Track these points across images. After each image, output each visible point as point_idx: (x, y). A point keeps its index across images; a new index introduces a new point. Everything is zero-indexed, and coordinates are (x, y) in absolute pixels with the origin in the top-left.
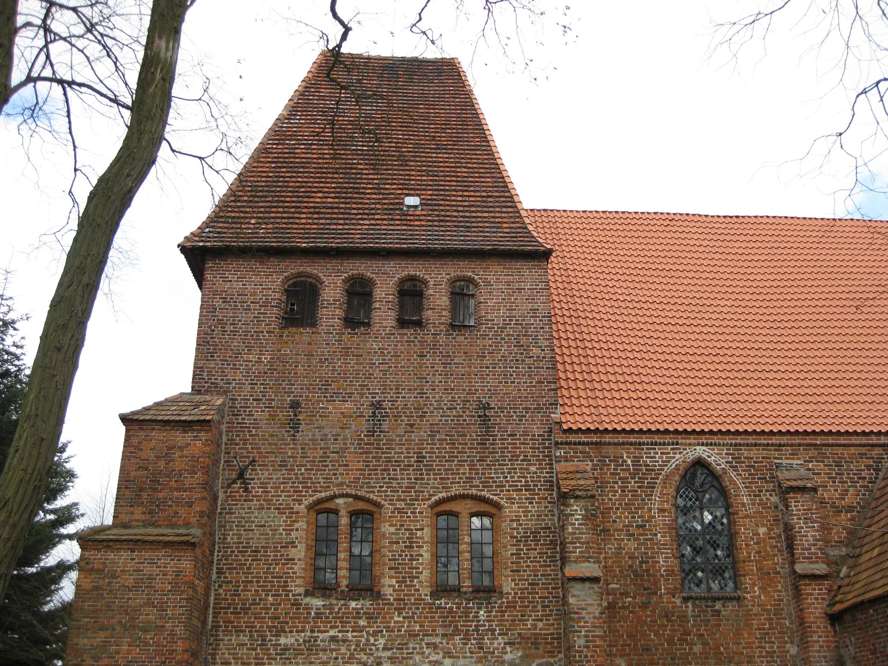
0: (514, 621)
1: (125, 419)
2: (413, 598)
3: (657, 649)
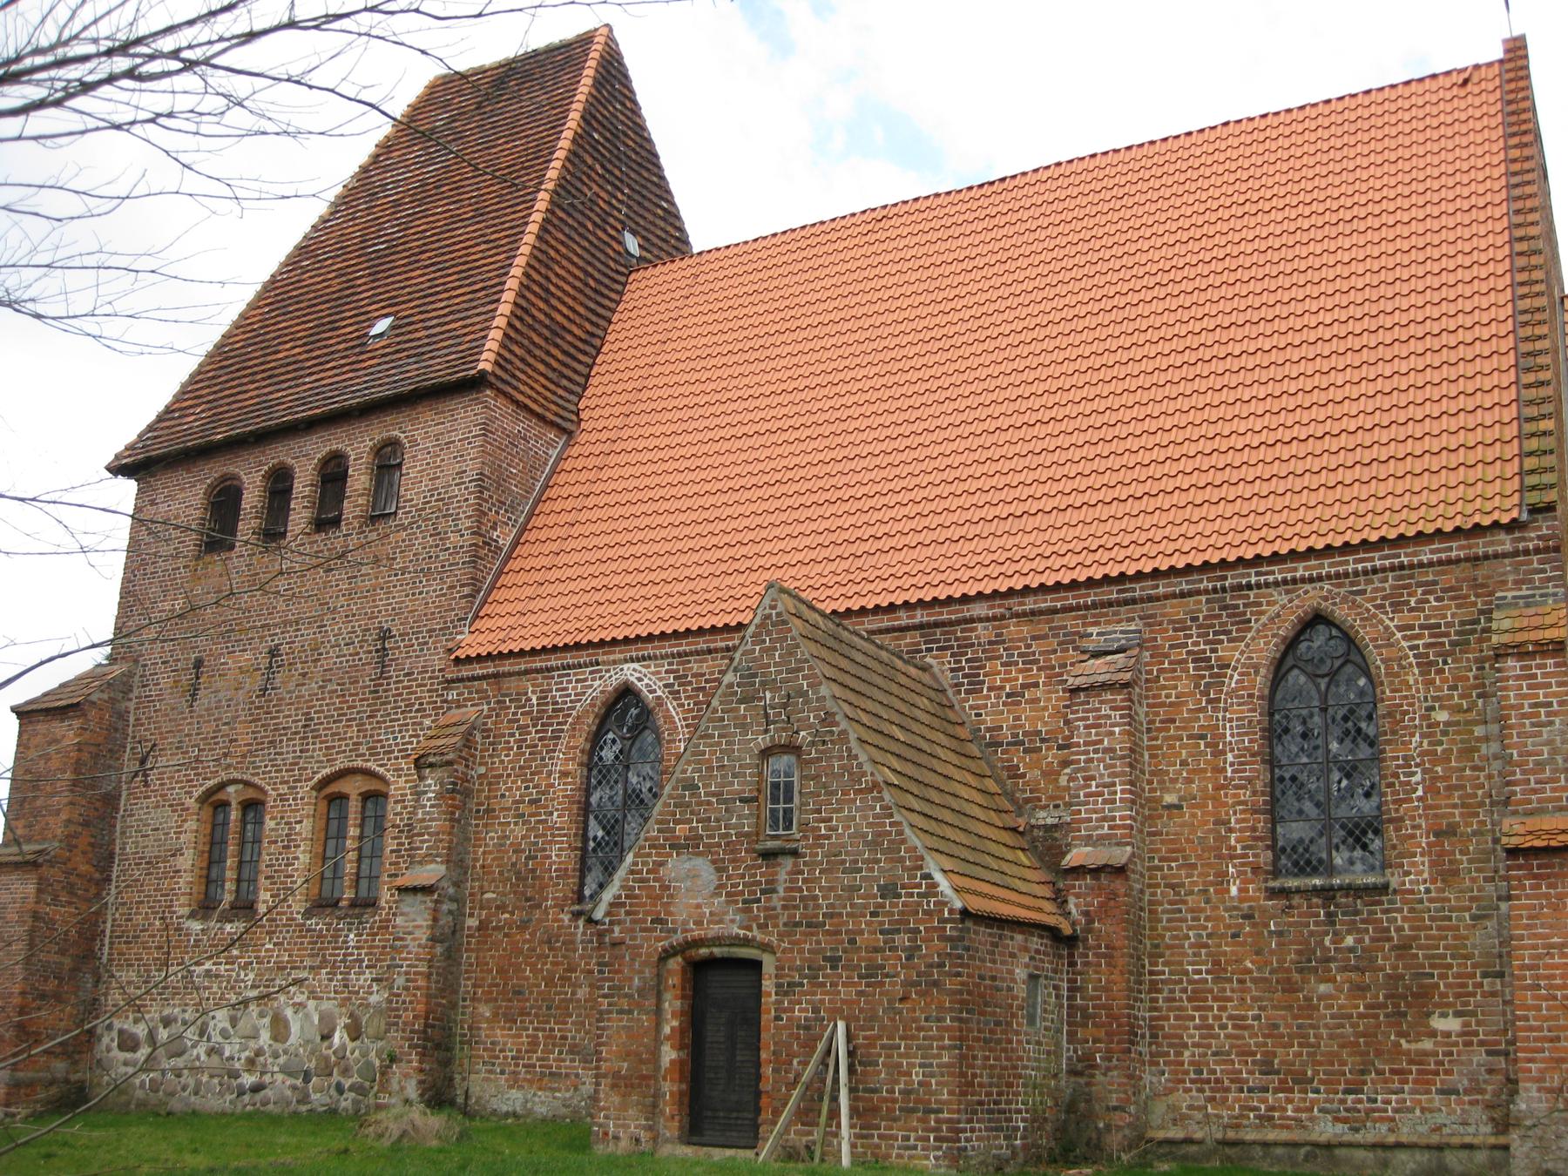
0: (384, 947)
1: (14, 709)
2: (1467, 915)
3: (531, 993)
